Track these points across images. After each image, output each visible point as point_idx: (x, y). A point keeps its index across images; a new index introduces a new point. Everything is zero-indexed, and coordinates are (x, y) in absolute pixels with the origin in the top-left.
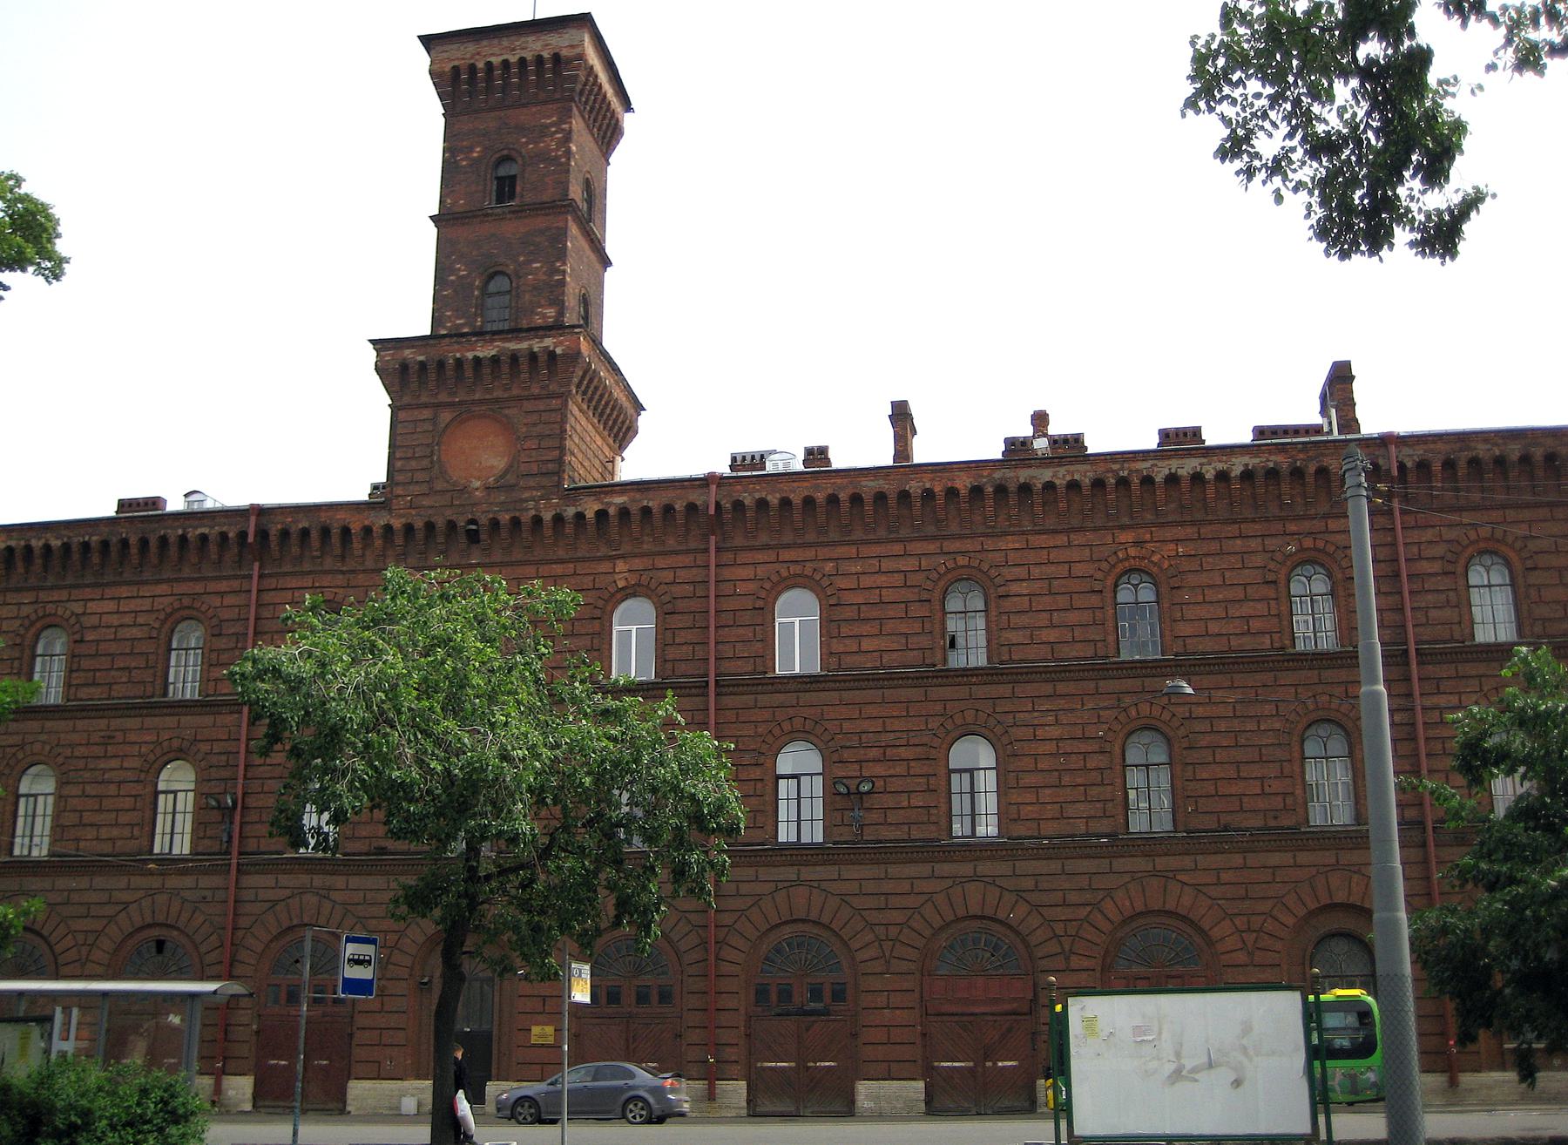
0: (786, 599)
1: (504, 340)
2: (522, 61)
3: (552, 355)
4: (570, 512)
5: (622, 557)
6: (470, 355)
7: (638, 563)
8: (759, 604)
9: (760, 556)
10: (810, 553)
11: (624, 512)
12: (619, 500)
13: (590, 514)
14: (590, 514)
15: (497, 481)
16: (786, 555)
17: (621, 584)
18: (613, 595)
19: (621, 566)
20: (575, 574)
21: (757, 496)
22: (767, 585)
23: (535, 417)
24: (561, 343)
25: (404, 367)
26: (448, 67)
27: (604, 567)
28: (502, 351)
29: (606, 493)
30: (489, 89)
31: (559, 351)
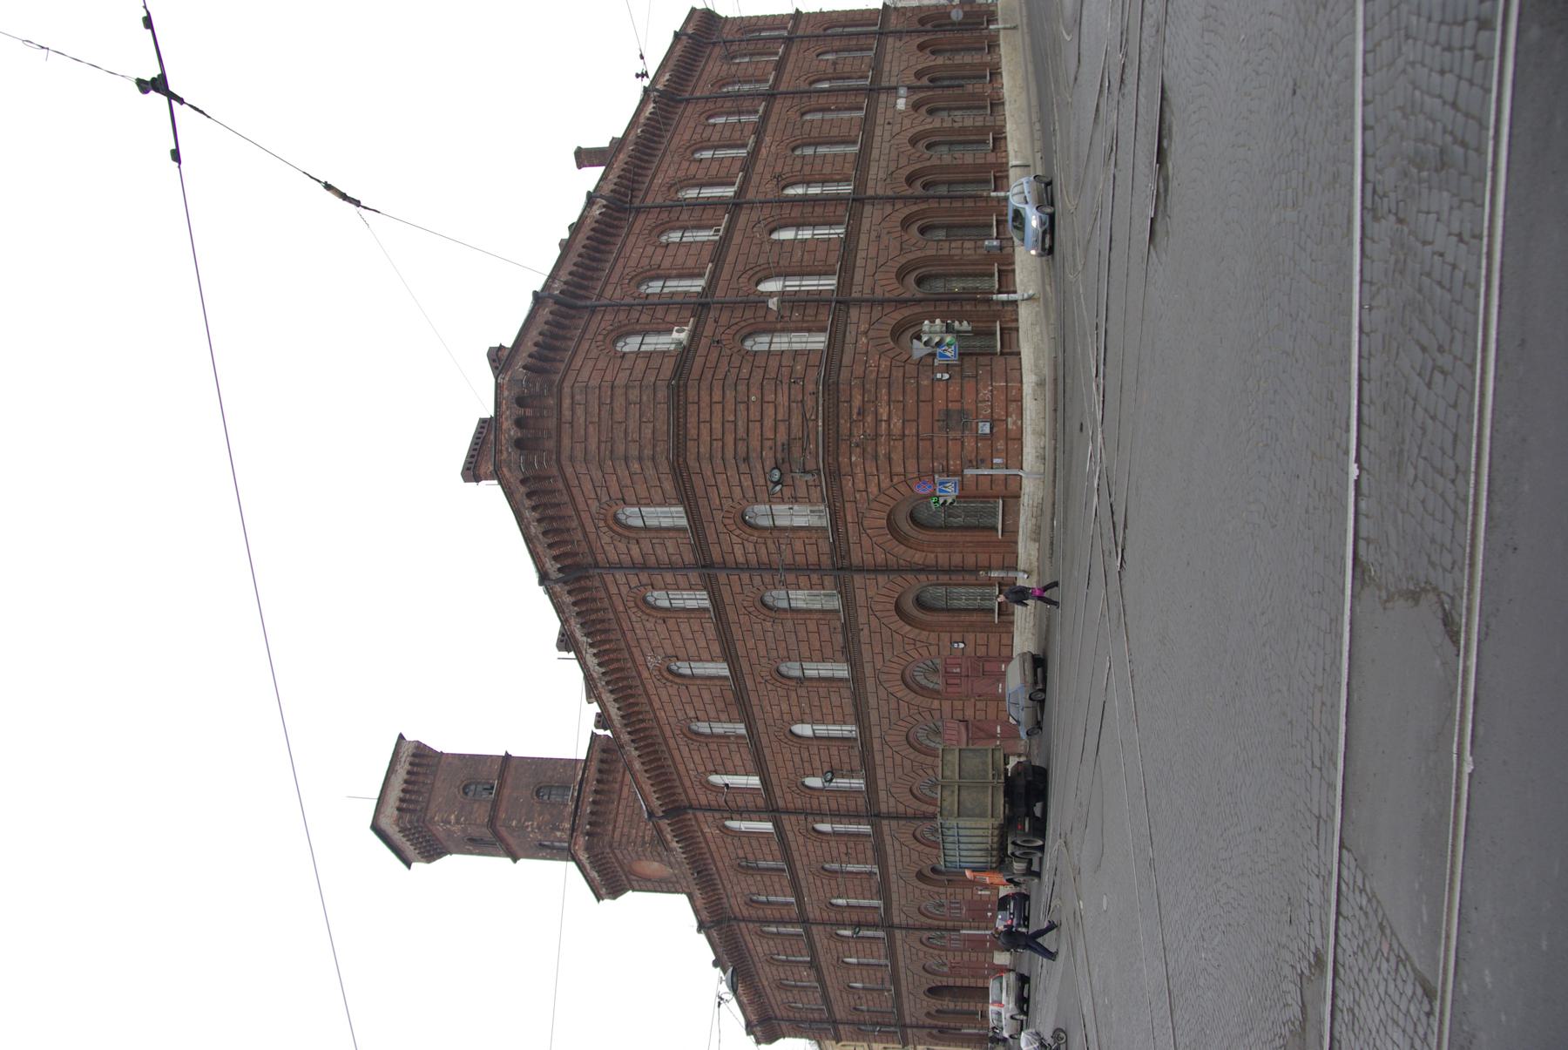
19: (706, 830)
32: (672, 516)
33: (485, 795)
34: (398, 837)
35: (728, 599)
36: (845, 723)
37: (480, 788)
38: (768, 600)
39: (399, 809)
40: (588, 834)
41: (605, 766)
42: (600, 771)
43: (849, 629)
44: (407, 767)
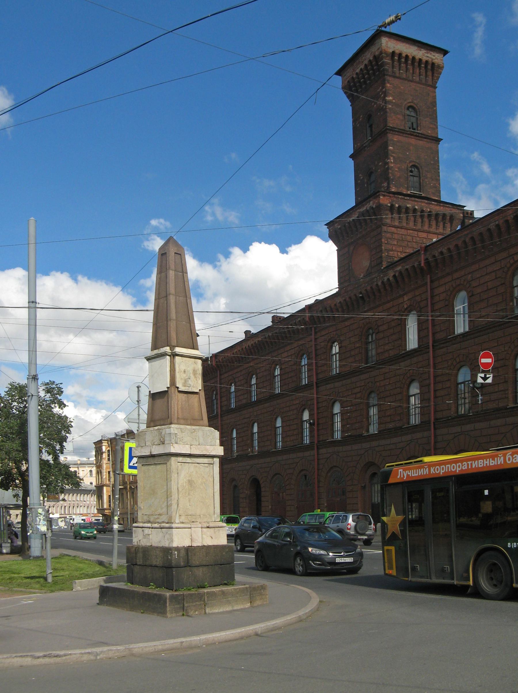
4: (386, 279)
12: (399, 268)
17: (405, 307)
19: (406, 298)
20: (393, 306)
27: (400, 300)
32: (461, 326)
33: (409, 124)
34: (368, 56)
35: (415, 360)
36: (282, 443)
37: (413, 120)
38: (373, 395)
39: (393, 53)
40: (392, 206)
41: (440, 218)
42: (437, 215)
43: (398, 431)
44: (424, 59)
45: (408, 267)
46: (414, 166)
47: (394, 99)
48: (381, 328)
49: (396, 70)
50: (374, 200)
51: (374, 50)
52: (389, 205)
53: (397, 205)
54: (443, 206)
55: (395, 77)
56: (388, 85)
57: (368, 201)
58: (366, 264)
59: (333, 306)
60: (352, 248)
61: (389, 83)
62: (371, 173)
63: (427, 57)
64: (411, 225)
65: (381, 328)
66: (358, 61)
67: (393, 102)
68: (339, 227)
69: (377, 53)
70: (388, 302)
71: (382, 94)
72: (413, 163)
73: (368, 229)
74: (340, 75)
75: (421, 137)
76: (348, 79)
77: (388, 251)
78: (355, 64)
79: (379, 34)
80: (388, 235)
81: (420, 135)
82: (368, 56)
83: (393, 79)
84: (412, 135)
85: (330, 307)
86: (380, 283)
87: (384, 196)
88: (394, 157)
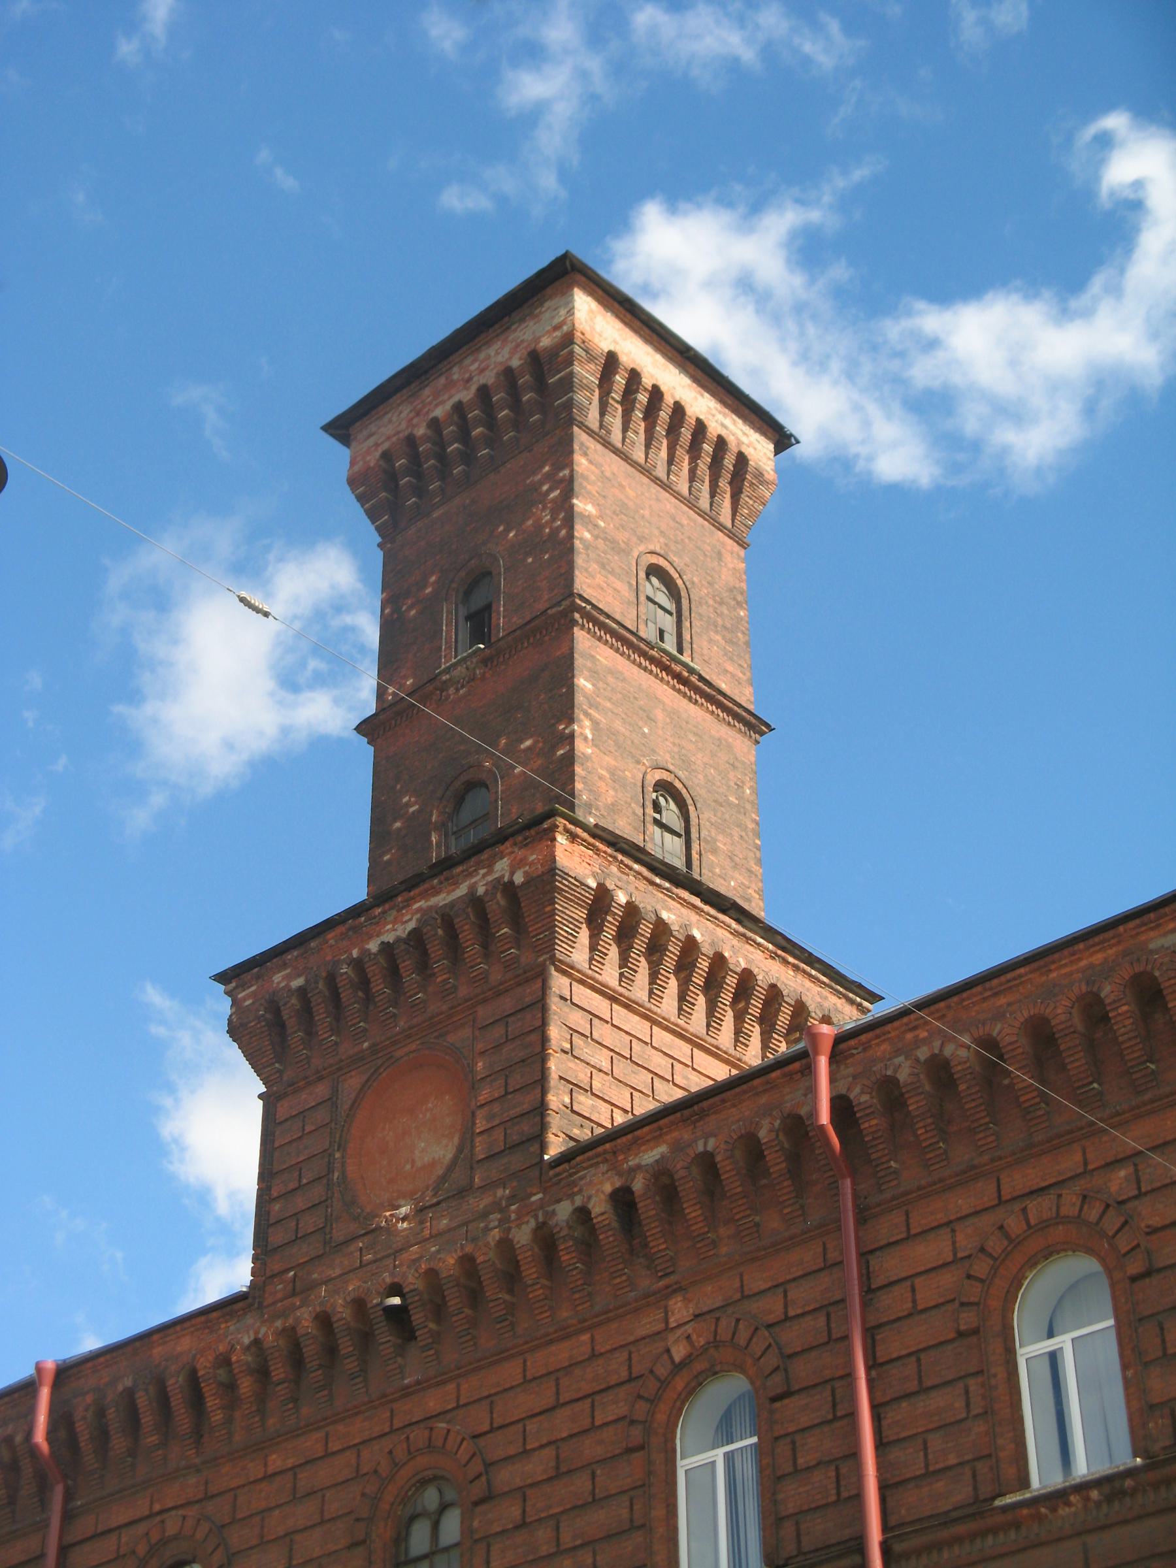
0: (1041, 1288)
1: (425, 895)
2: (484, 393)
3: (509, 889)
4: (564, 1211)
5: (678, 1289)
6: (373, 946)
7: (710, 1296)
8: (968, 1319)
9: (962, 1202)
10: (1071, 1161)
11: (665, 1184)
12: (651, 1156)
13: (599, 1207)
14: (599, 1207)
15: (436, 1190)
16: (1017, 1181)
17: (679, 1352)
18: (664, 1384)
19: (680, 1310)
20: (594, 1356)
21: (923, 1053)
22: (981, 1268)
23: (498, 1032)
24: (521, 863)
25: (274, 1007)
26: (373, 459)
27: (648, 1323)
28: (426, 917)
29: (628, 1149)
30: (443, 471)
31: (519, 878)
34: (502, 354)
45: (711, 1144)
46: (663, 787)
47: (601, 517)
48: (506, 1477)
49: (615, 422)
50: (520, 853)
51: (536, 332)
52: (594, 885)
53: (622, 898)
54: (796, 968)
55: (607, 444)
56: (584, 461)
57: (484, 856)
58: (434, 1150)
59: (204, 1365)
60: (352, 1083)
61: (585, 454)
62: (471, 786)
63: (723, 425)
64: (668, 1006)
65: (506, 1477)
66: (442, 380)
67: (596, 526)
68: (298, 982)
69: (545, 342)
70: (566, 1334)
71: (551, 490)
72: (668, 777)
73: (463, 991)
74: (345, 440)
75: (697, 690)
76: (386, 446)
77: (574, 1087)
78: (427, 391)
79: (564, 273)
80: (578, 1020)
81: (694, 679)
82: (502, 354)
83: (599, 447)
84: (666, 669)
85: (193, 1379)
86: (523, 1235)
87: (573, 837)
88: (596, 724)
